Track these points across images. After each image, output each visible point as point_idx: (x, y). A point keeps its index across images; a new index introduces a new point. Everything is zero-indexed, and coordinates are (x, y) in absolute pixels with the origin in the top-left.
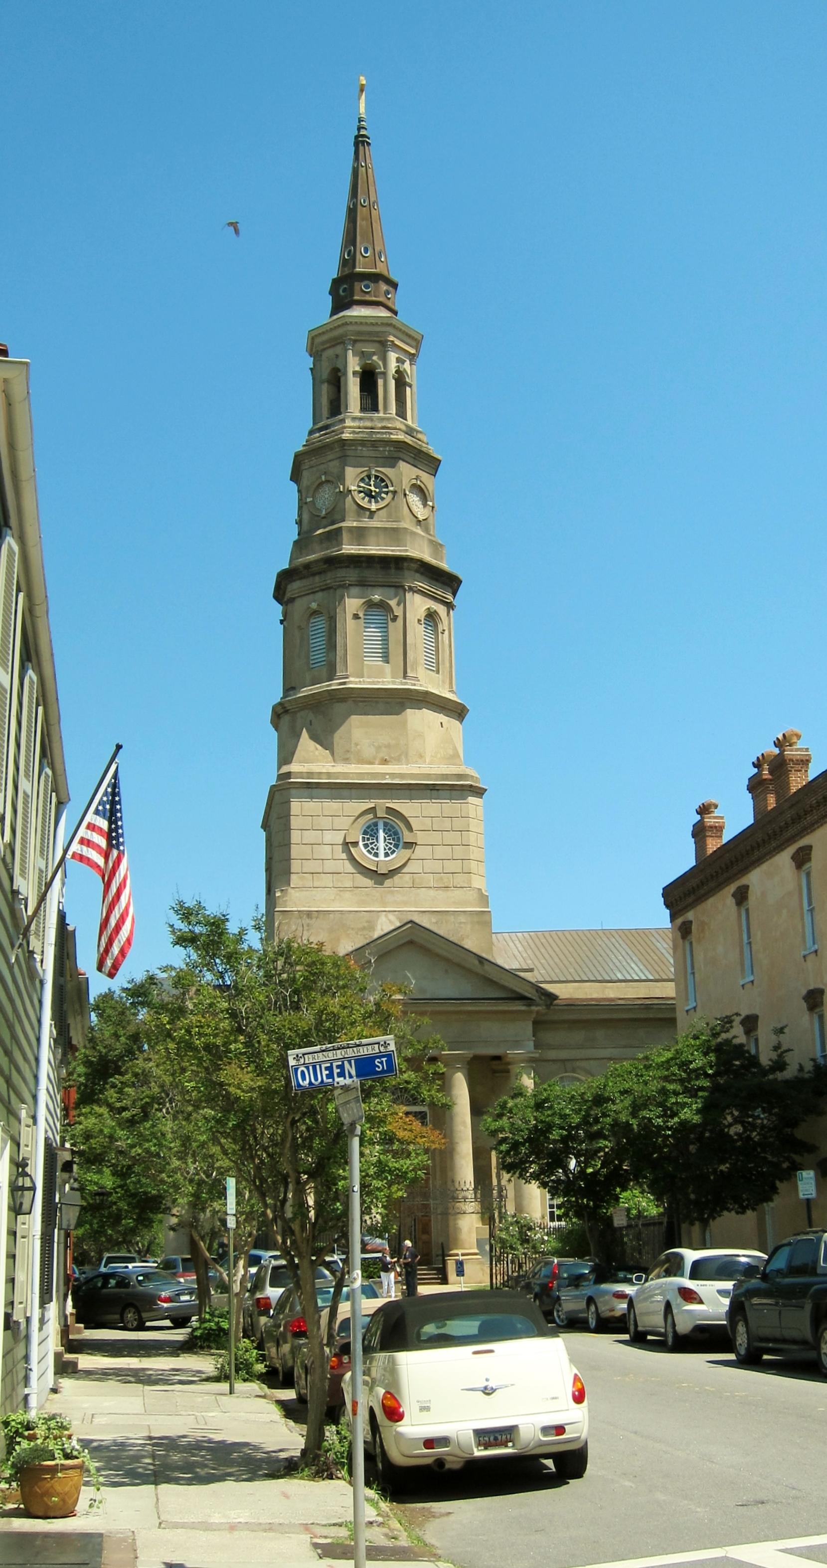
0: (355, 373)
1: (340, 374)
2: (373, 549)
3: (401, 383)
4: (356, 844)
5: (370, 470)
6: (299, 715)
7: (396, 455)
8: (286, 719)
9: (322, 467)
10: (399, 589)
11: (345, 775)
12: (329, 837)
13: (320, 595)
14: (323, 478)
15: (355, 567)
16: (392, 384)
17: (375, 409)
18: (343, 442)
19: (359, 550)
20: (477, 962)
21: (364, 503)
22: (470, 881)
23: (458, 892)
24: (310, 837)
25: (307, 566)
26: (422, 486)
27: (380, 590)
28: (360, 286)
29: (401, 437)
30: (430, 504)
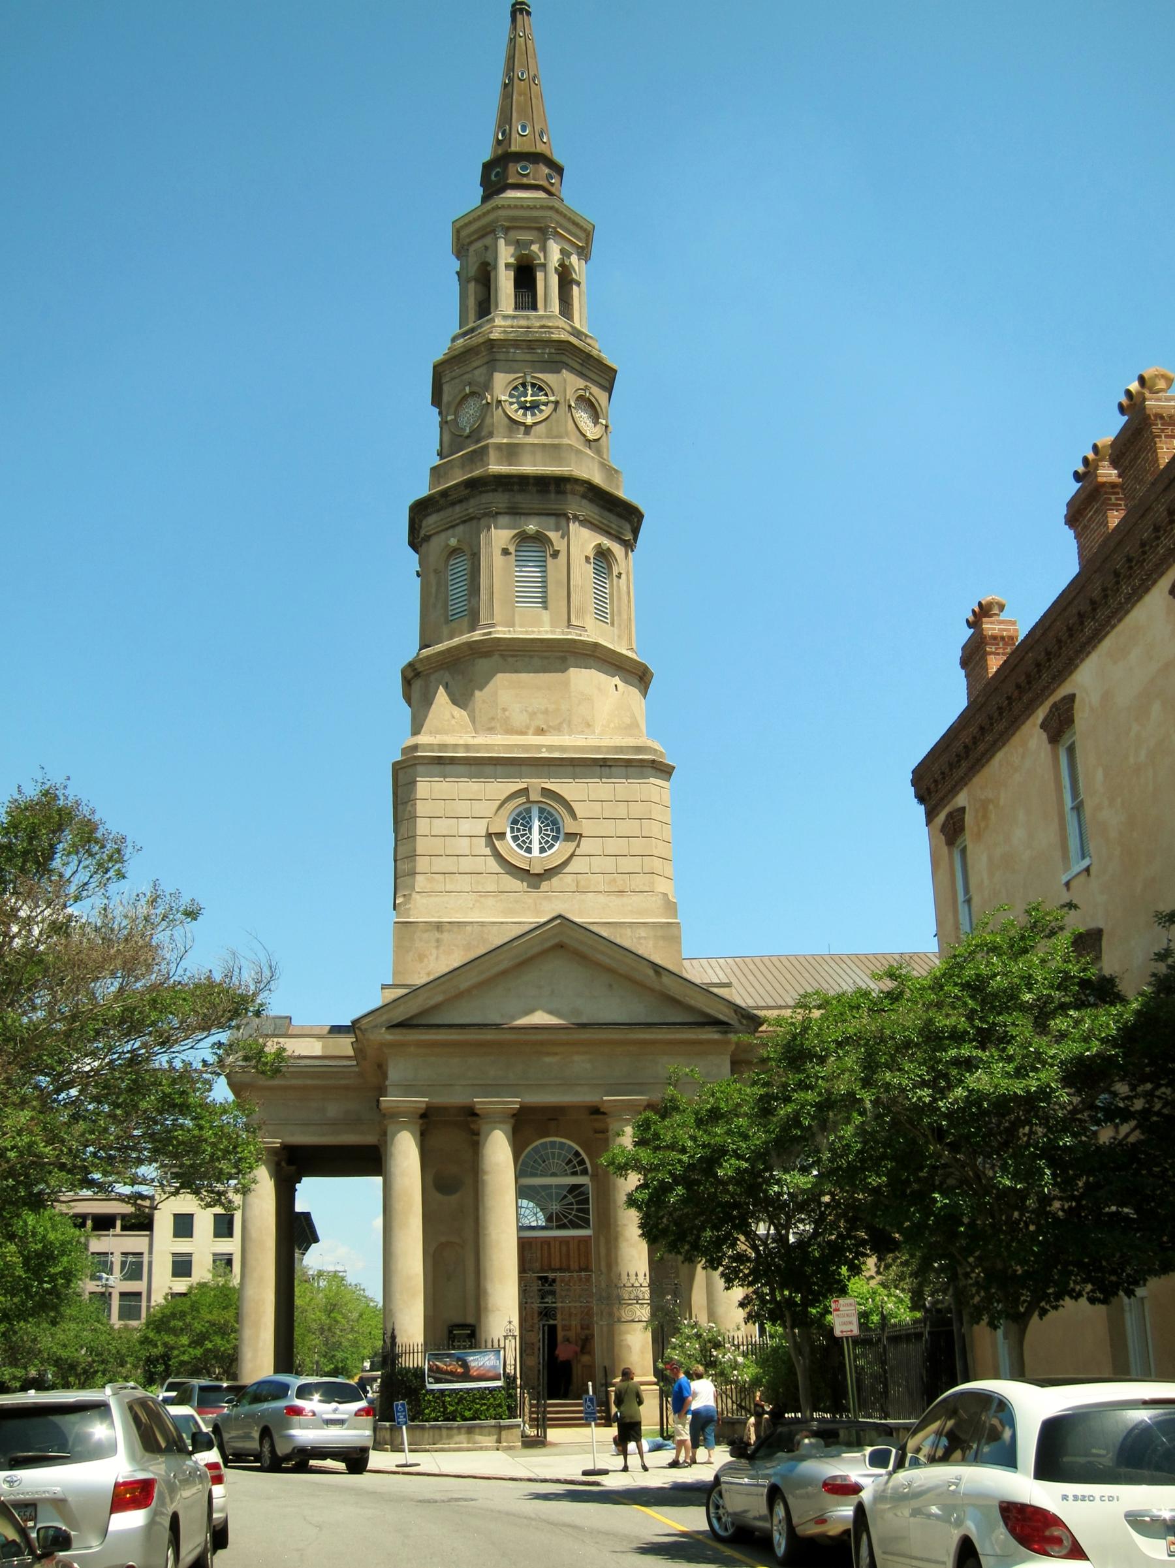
0: (507, 266)
2: (528, 467)
3: (566, 280)
4: (501, 836)
5: (524, 377)
7: (558, 358)
8: (417, 685)
9: (466, 376)
10: (561, 518)
11: (488, 747)
12: (466, 827)
13: (460, 529)
14: (467, 390)
15: (503, 491)
16: (554, 280)
17: (534, 307)
18: (491, 344)
20: (651, 972)
21: (518, 416)
23: (636, 898)
24: (441, 826)
25: (444, 494)
26: (593, 400)
27: (536, 519)
29: (563, 336)
30: (604, 422)
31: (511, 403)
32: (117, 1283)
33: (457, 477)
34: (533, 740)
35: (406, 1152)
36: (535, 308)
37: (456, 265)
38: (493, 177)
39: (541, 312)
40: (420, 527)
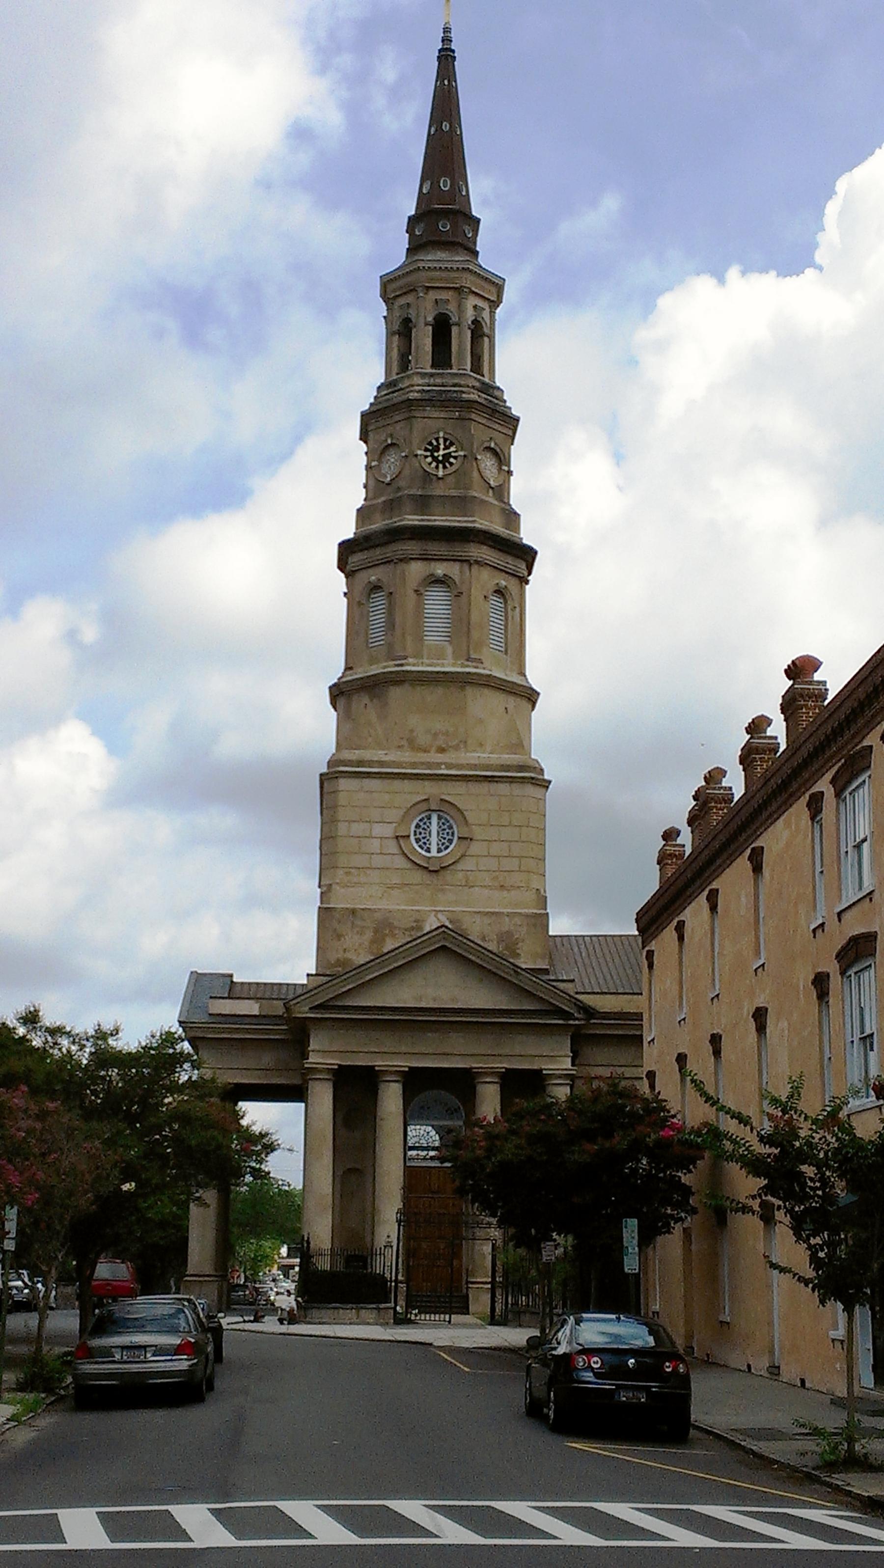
6: (355, 697)
8: (341, 702)
19: (423, 520)
24: (357, 829)
26: (498, 450)
31: (426, 457)
33: (378, 524)
34: (435, 757)
37: (383, 310)
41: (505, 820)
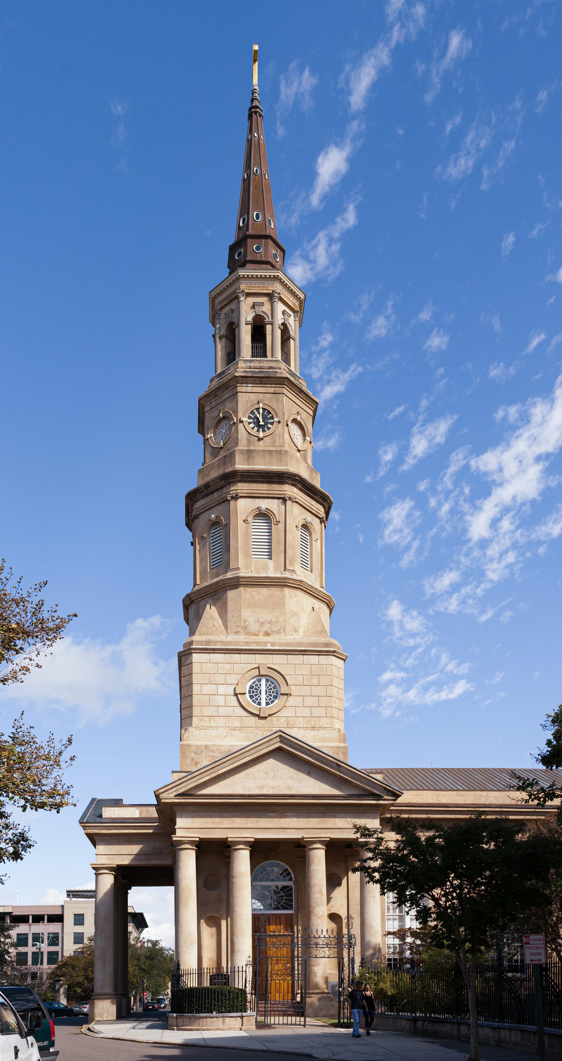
1: (234, 326)
12: (222, 689)
16: (278, 333)
21: (254, 432)
22: (332, 724)
24: (208, 689)
25: (207, 486)
28: (253, 246)
31: (250, 423)
32: (45, 948)
33: (215, 474)
35: (188, 864)
36: (265, 356)
38: (237, 258)
39: (269, 358)
40: (192, 510)
41: (315, 681)
